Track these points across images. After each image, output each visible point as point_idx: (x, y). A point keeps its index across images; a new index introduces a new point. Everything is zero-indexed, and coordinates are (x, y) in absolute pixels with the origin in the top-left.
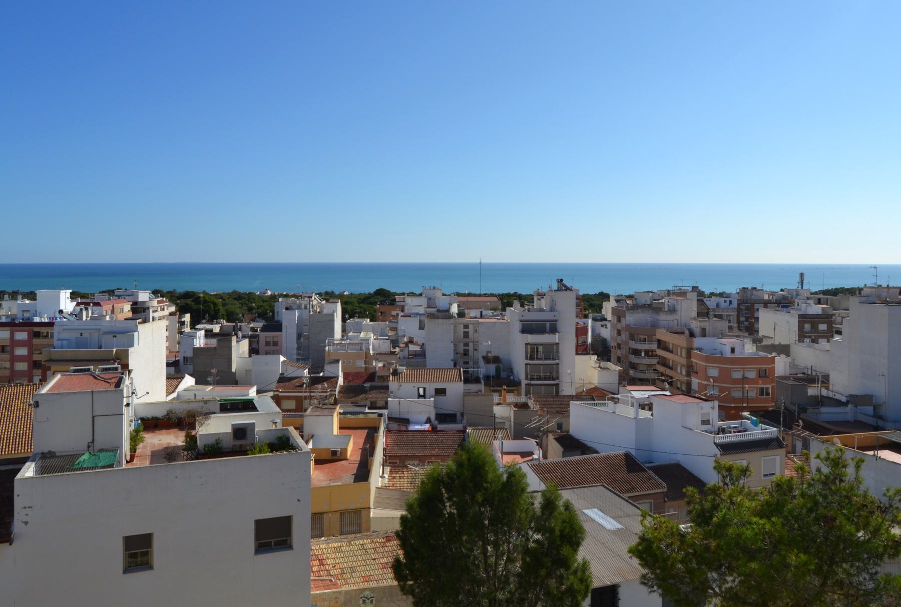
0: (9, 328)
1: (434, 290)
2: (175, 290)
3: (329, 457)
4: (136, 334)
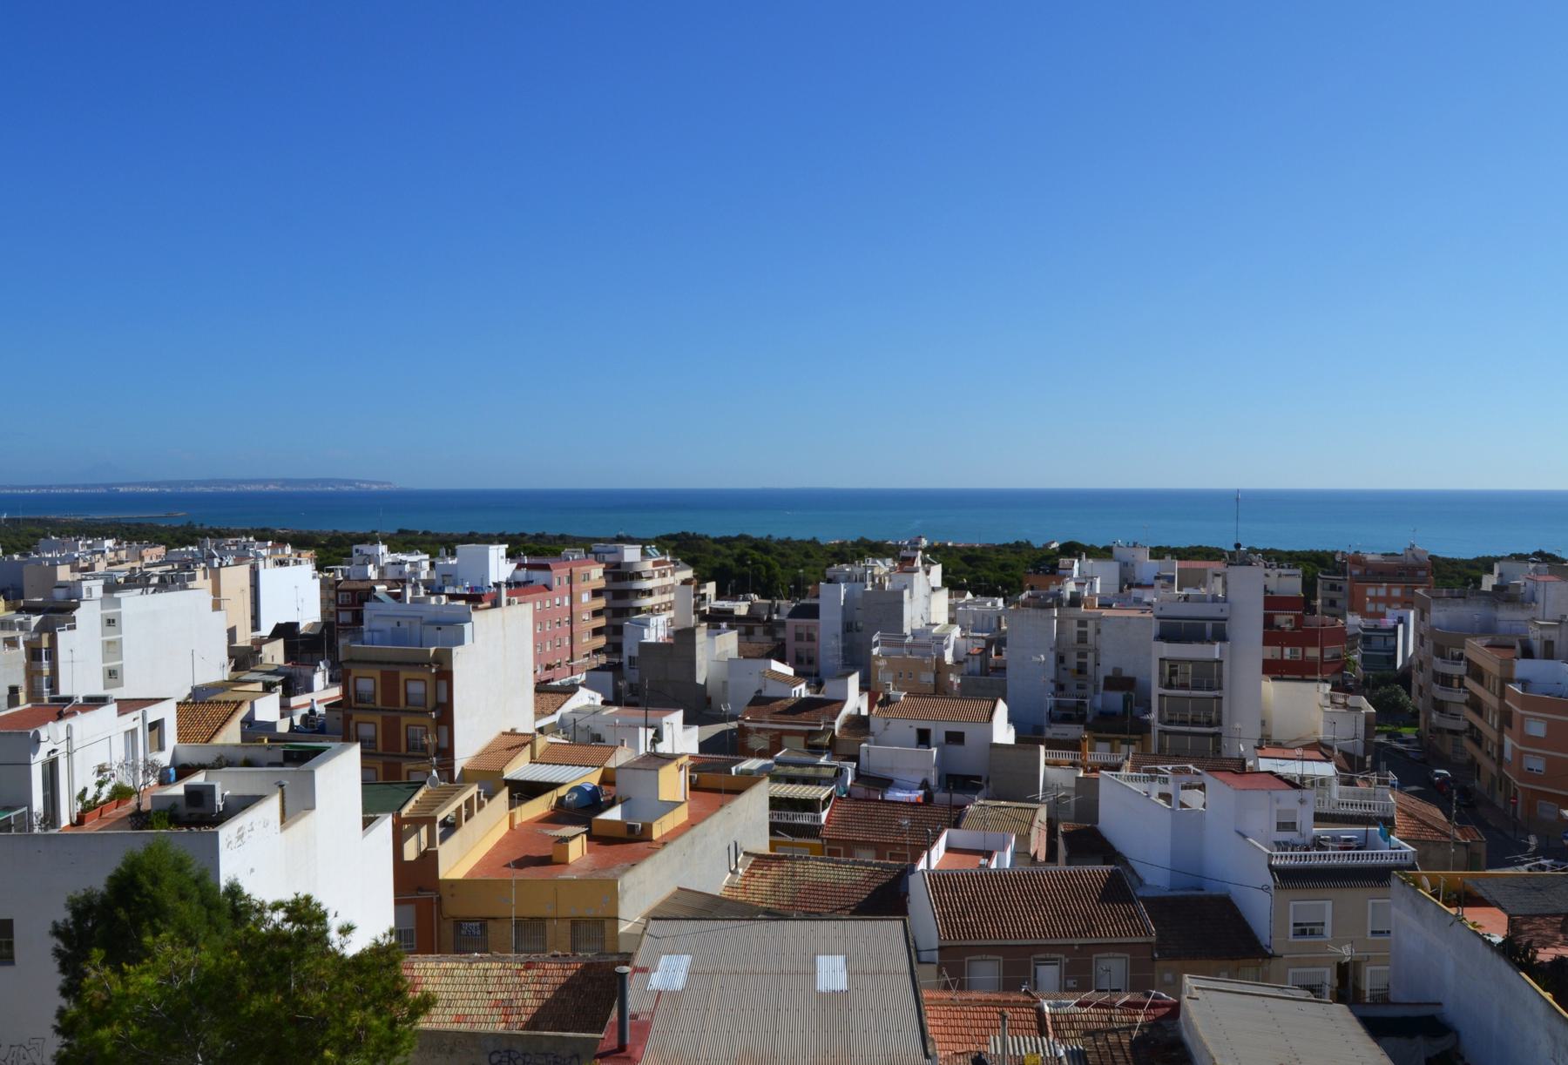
1: (1133, 550)
2: (770, 536)
3: (623, 833)
4: (467, 627)
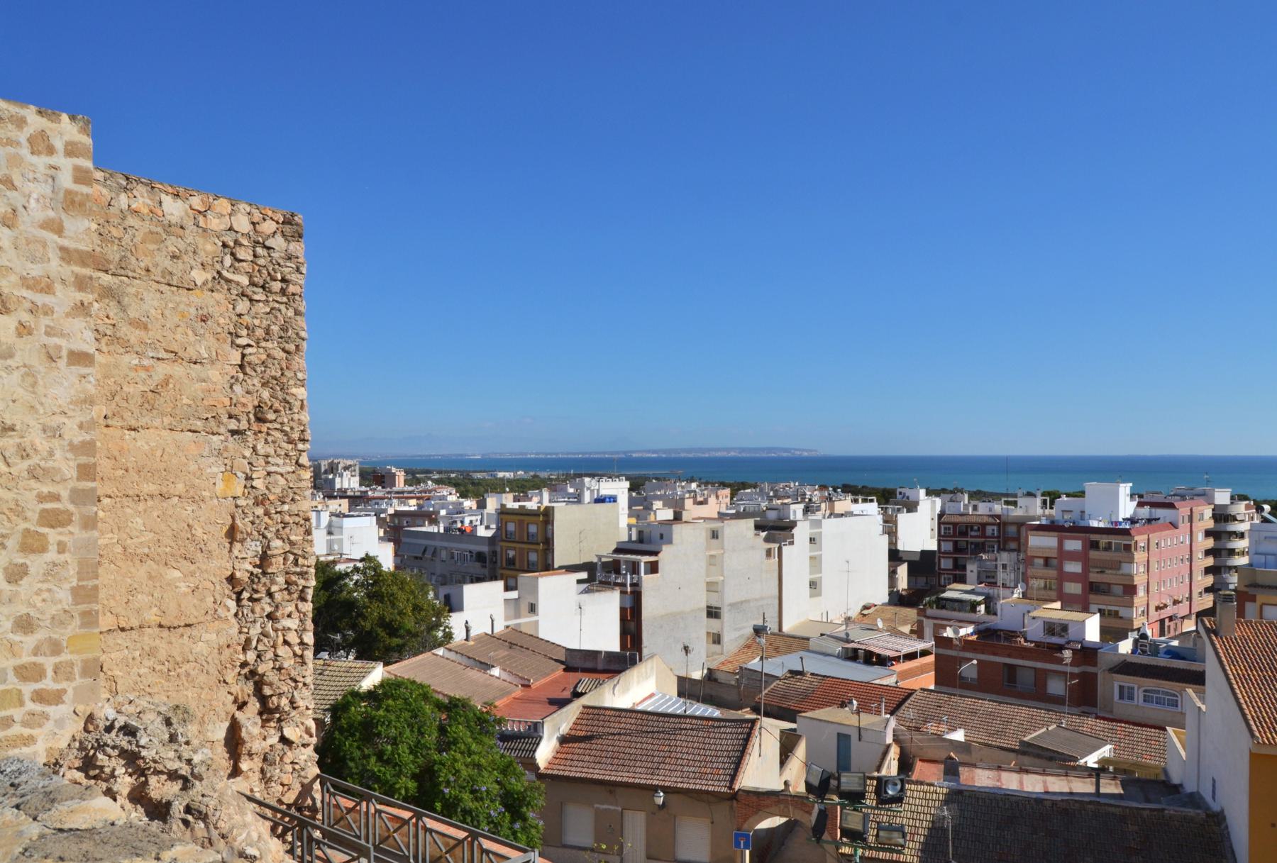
0: (1056, 534)
